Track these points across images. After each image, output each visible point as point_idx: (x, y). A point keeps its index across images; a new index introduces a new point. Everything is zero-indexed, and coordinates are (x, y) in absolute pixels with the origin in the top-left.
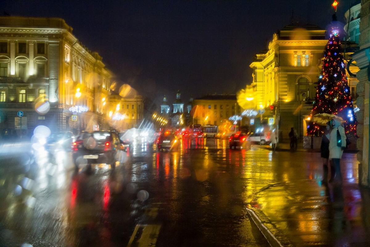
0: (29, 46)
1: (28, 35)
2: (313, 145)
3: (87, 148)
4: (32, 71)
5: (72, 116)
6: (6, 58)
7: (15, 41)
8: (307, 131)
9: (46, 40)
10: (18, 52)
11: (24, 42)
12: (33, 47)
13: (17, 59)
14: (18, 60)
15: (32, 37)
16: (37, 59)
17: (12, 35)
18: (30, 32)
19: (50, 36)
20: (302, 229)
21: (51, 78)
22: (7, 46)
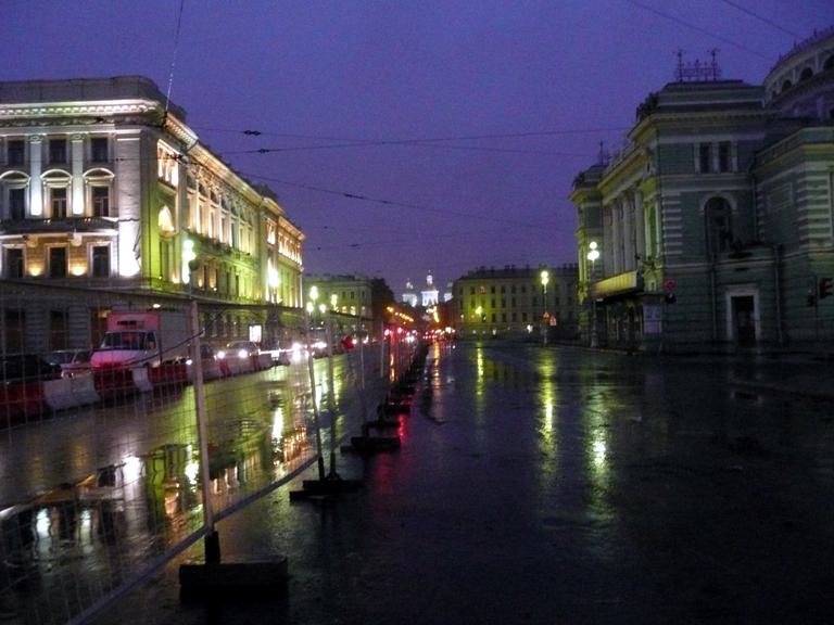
0: (29, 144)
1: (70, 120)
2: (500, 267)
3: (145, 508)
4: (78, 204)
5: (653, 169)
6: (23, 177)
7: (41, 136)
8: (387, 284)
9: (110, 130)
10: (90, 157)
11: (21, 139)
12: (81, 149)
13: (49, 176)
14: (49, 180)
15: (79, 124)
16: (49, 176)
17: (33, 123)
18: (73, 113)
19: (120, 120)
20: (610, 510)
21: (122, 218)
22: (65, 145)
